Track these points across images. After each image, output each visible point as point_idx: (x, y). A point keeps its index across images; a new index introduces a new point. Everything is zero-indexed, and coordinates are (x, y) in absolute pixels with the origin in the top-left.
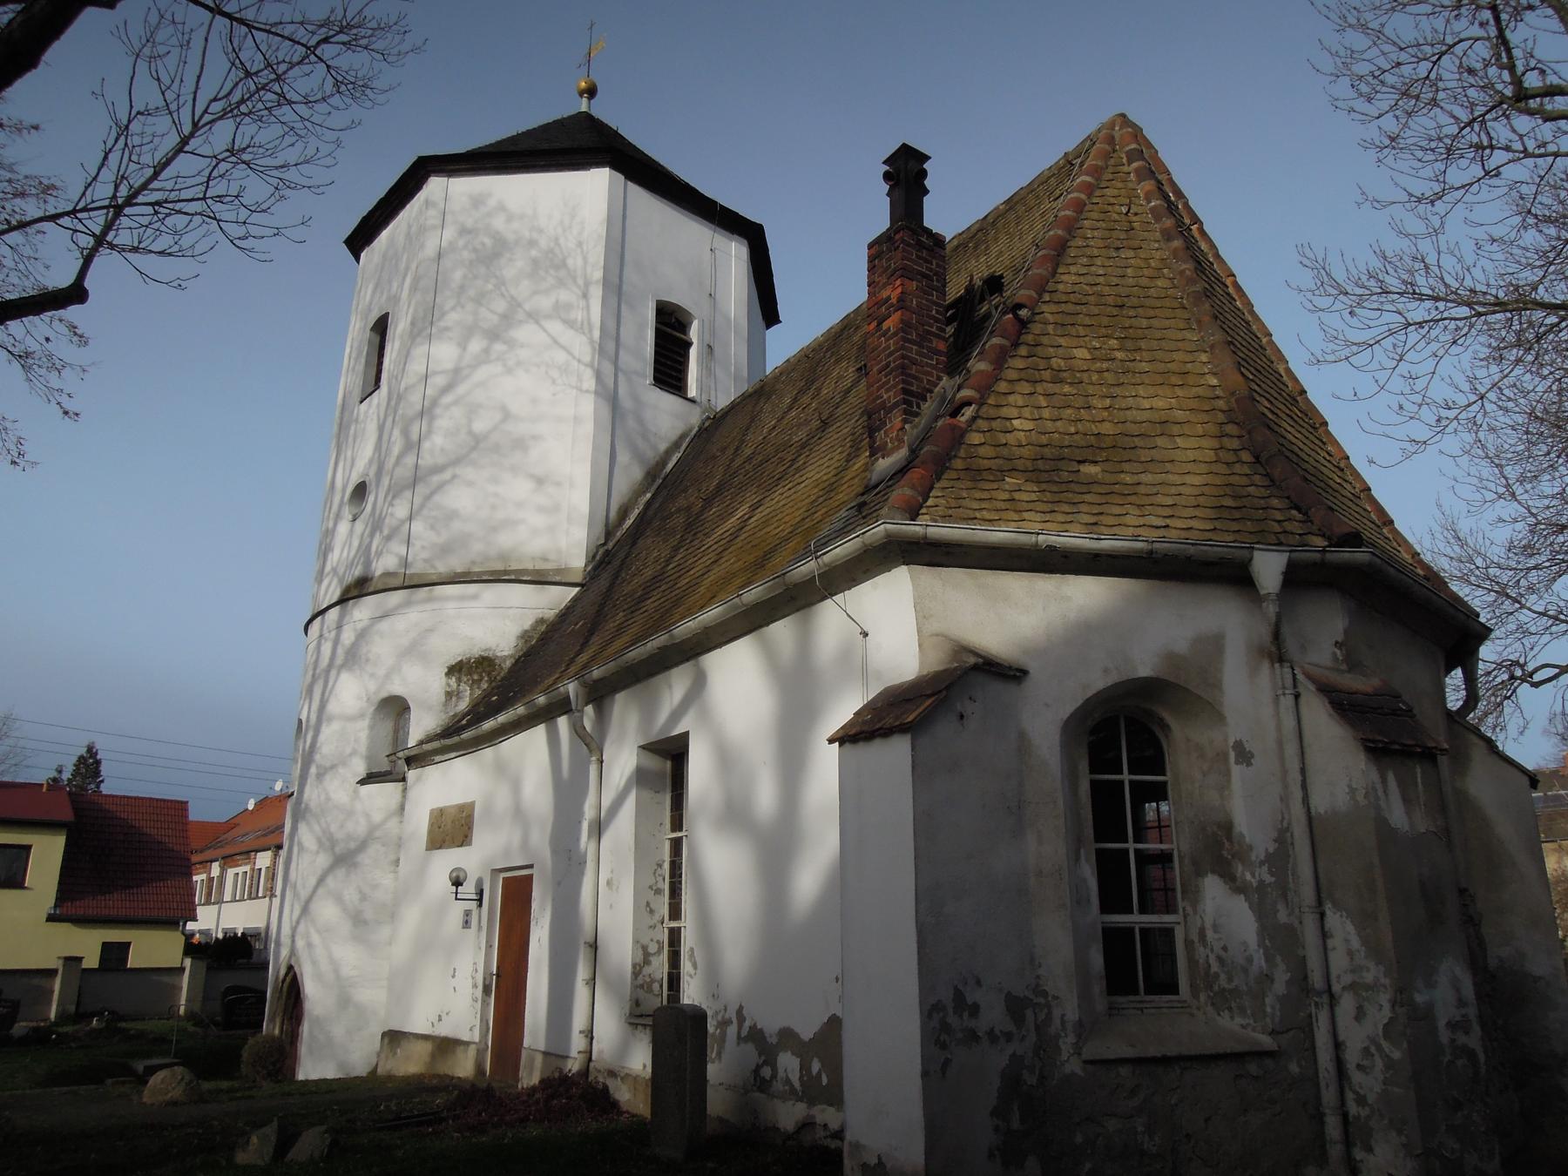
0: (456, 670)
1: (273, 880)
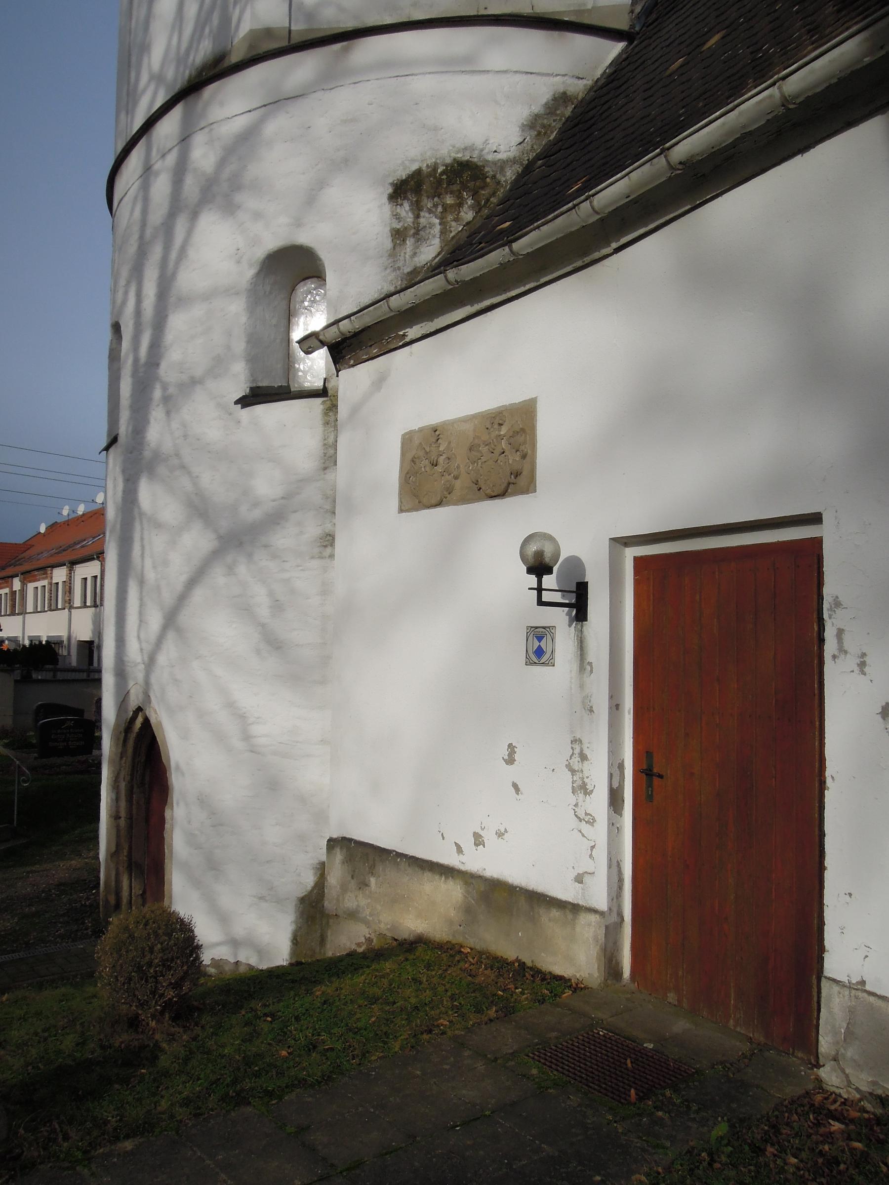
1: (70, 592)
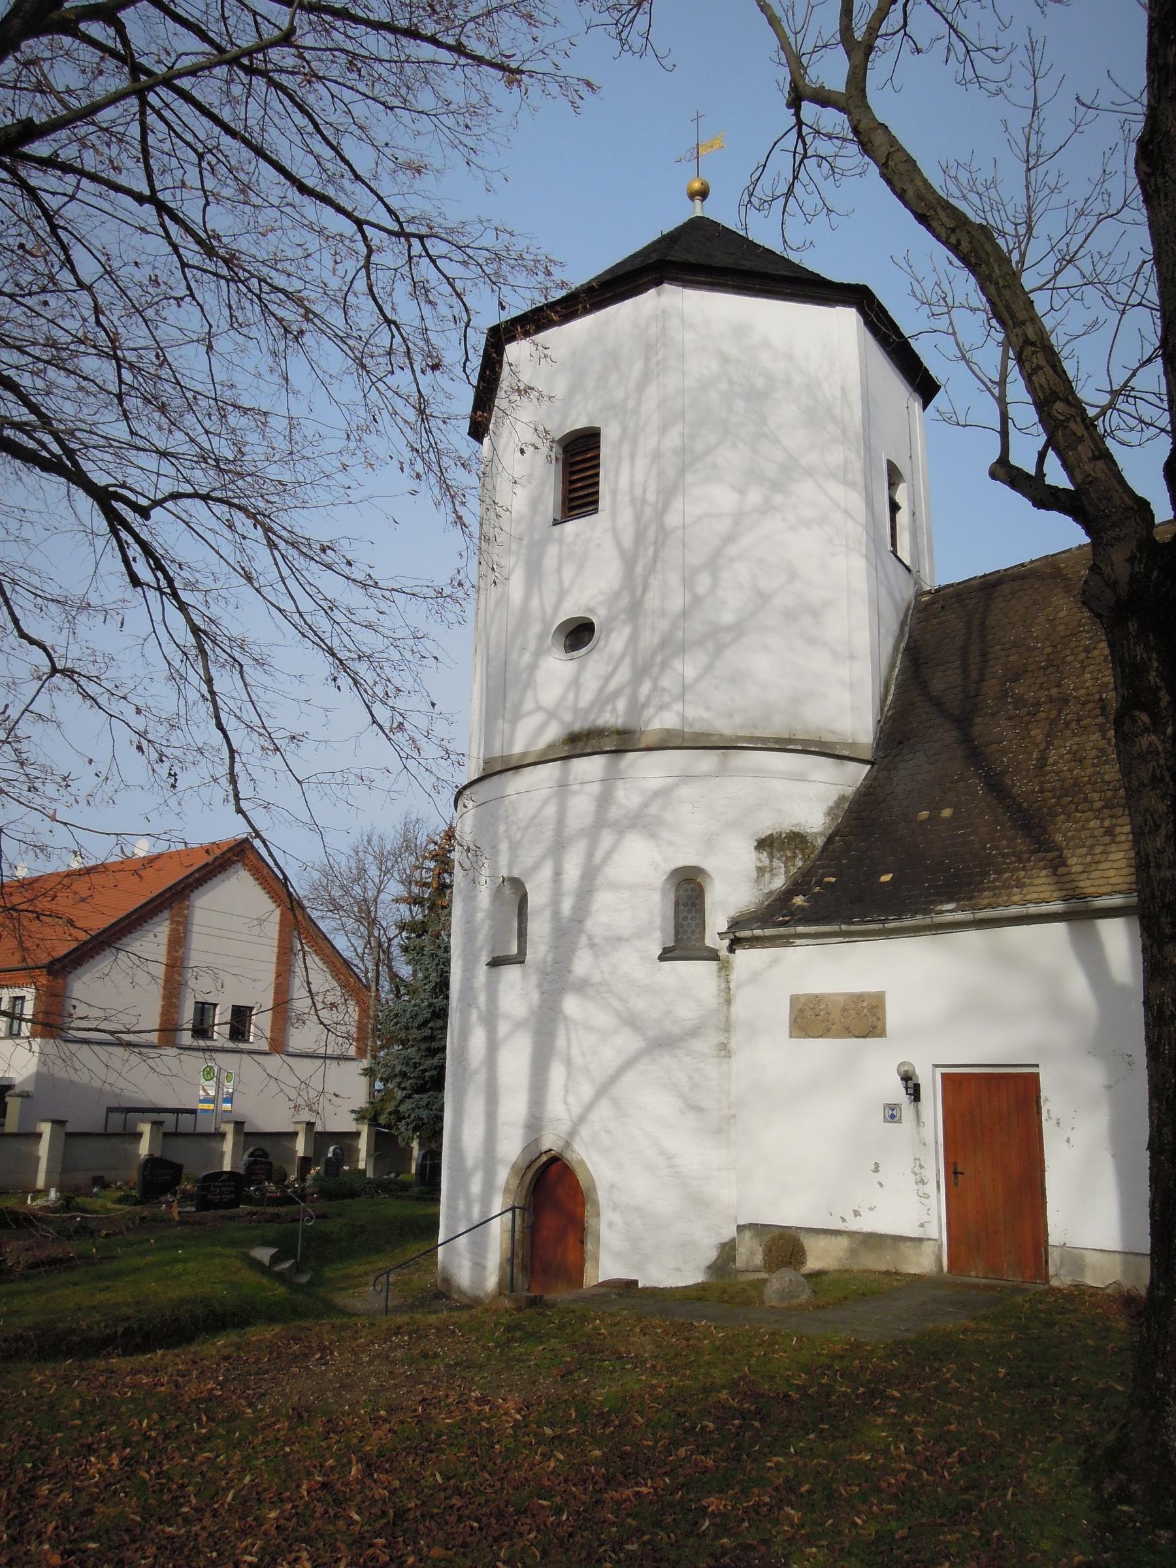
0: (765, 844)
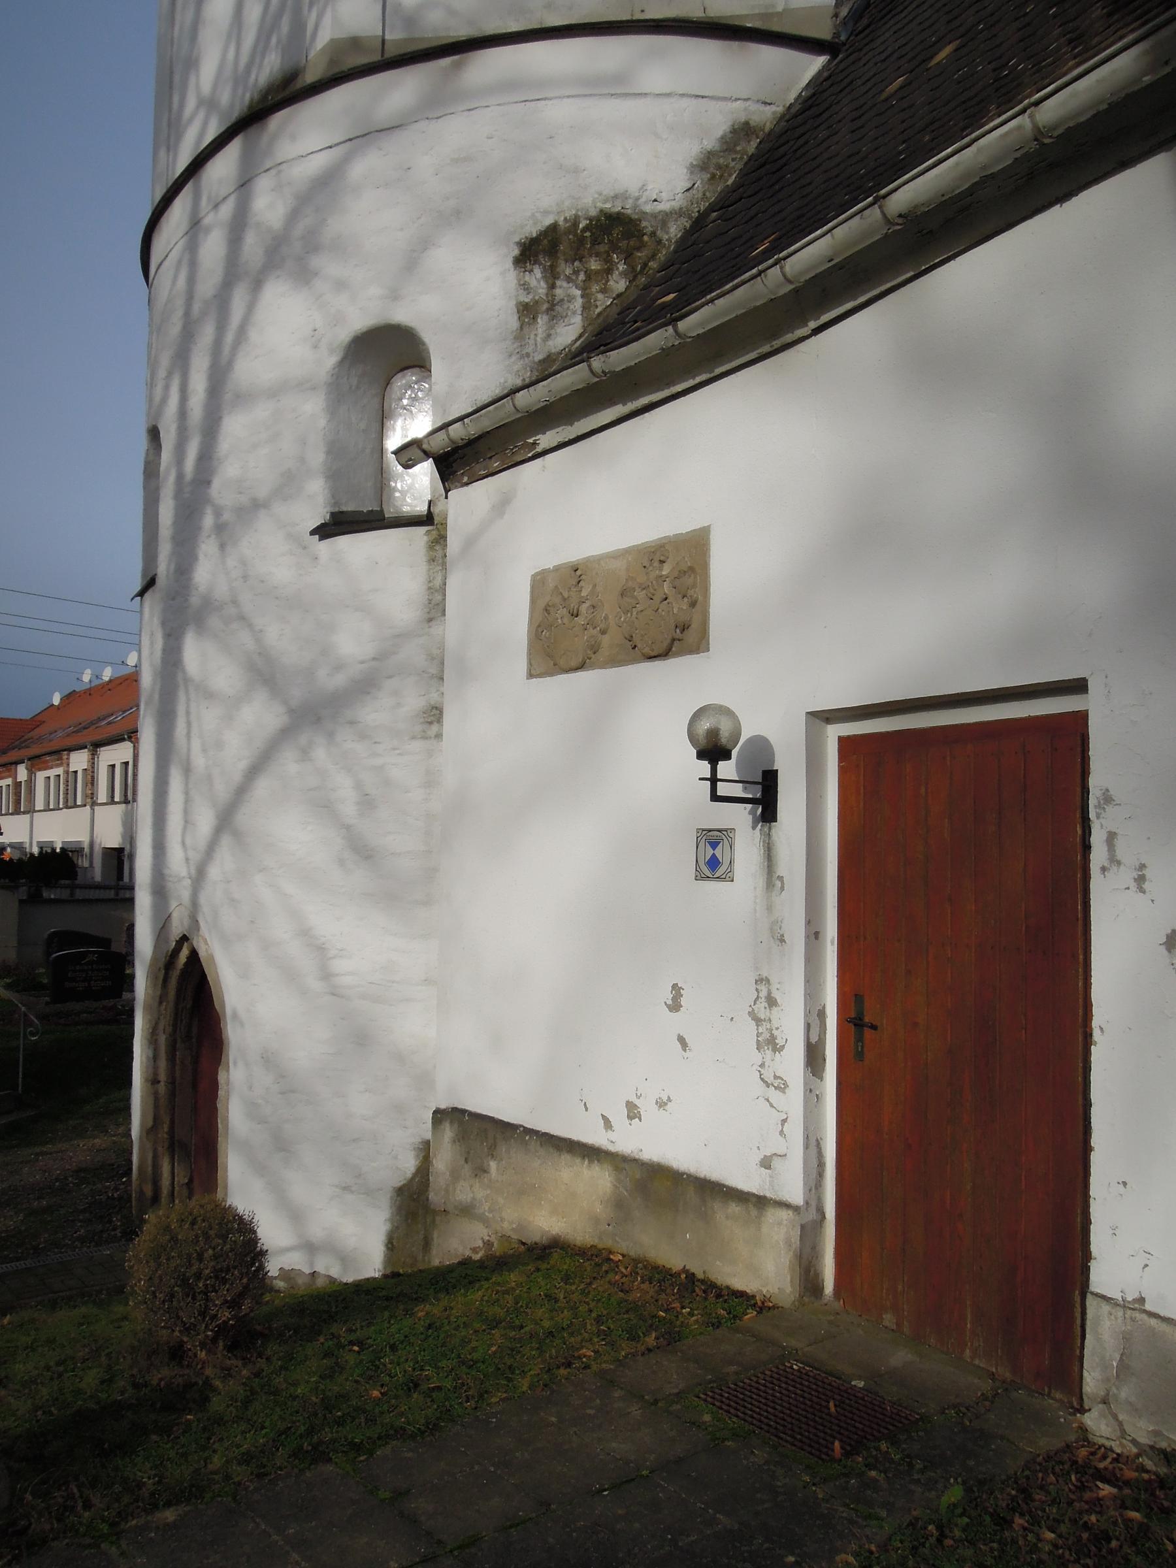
1: (92, 784)
